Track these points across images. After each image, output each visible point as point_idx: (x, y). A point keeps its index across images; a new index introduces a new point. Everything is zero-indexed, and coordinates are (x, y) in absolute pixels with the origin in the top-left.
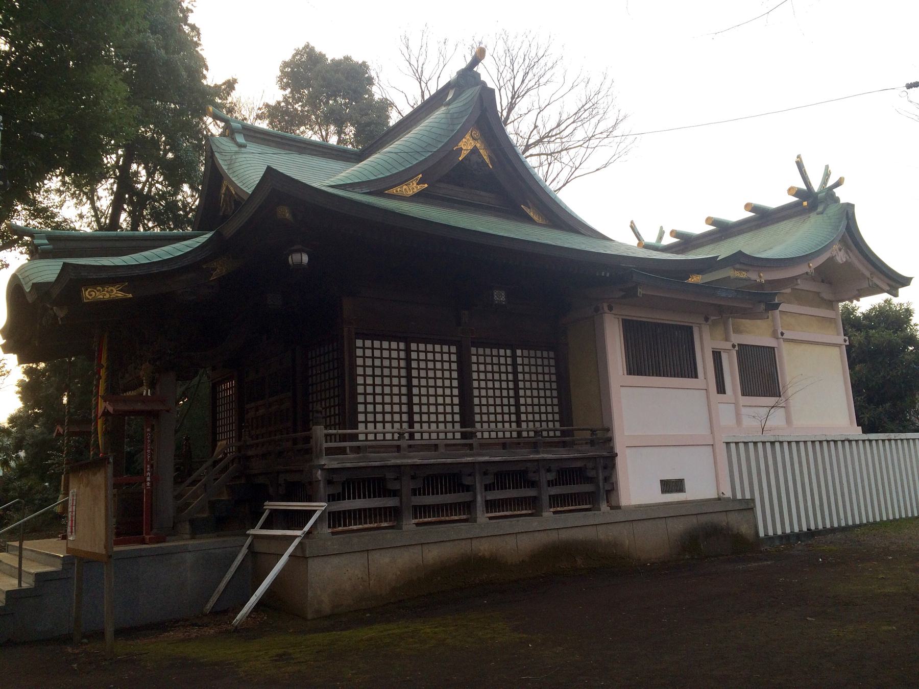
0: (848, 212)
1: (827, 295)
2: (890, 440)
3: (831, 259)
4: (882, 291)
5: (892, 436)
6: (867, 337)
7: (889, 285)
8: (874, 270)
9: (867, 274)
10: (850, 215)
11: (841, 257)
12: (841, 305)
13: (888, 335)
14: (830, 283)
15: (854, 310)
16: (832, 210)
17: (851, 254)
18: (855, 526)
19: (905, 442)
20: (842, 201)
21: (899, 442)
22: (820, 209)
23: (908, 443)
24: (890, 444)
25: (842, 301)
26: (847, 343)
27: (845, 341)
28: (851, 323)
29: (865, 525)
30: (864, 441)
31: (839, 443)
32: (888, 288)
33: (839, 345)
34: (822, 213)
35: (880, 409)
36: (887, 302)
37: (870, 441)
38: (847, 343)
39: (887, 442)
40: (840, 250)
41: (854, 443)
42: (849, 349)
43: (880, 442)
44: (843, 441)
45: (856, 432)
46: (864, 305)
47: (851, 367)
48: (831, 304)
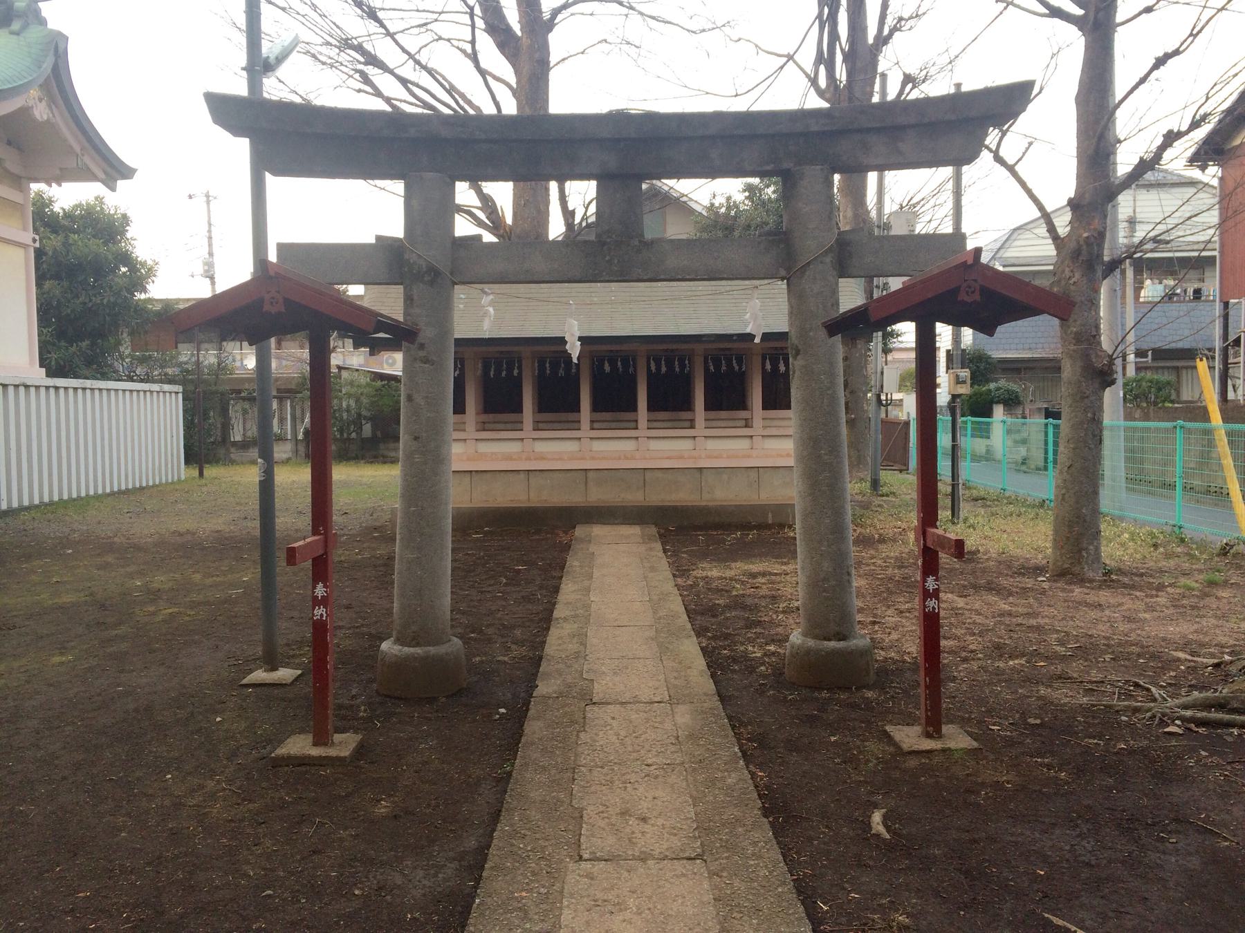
0: (57, 47)
1: (15, 168)
2: (84, 389)
3: (25, 112)
4: (94, 178)
5: (88, 383)
6: (66, 244)
7: (105, 173)
8: (87, 145)
9: (77, 148)
10: (61, 50)
11: (41, 112)
12: (35, 187)
13: (96, 246)
14: (19, 149)
15: (51, 201)
16: (34, 33)
17: (57, 114)
18: (22, 509)
19: (105, 393)
20: (50, 26)
21: (97, 392)
22: (16, 26)
23: (93, 394)
24: (109, 396)
25: (37, 180)
26: (37, 245)
27: (34, 241)
28: (45, 220)
29: (37, 506)
30: (47, 388)
31: (11, 389)
32: (103, 176)
33: (23, 246)
34: (17, 34)
35: (74, 349)
36: (99, 199)
37: (57, 388)
38: (37, 245)
39: (80, 391)
40: (40, 100)
41: (33, 390)
42: (39, 253)
43: (71, 391)
44: (16, 386)
45: (38, 375)
46: (67, 196)
47: (39, 285)
48: (19, 182)
